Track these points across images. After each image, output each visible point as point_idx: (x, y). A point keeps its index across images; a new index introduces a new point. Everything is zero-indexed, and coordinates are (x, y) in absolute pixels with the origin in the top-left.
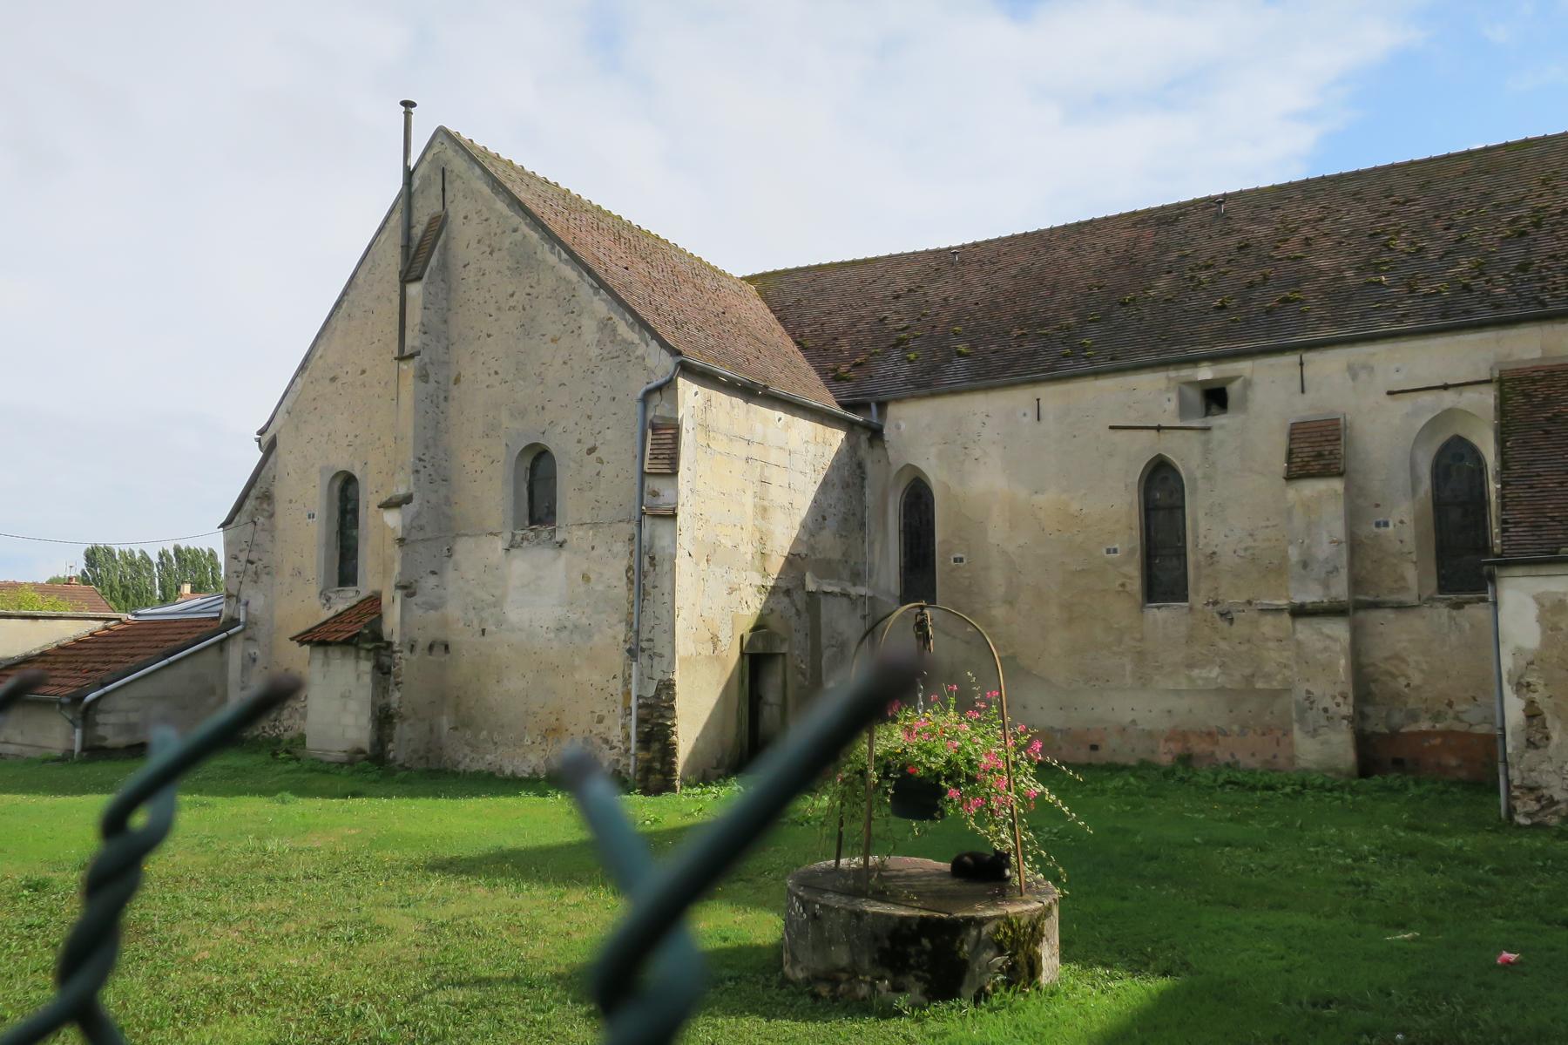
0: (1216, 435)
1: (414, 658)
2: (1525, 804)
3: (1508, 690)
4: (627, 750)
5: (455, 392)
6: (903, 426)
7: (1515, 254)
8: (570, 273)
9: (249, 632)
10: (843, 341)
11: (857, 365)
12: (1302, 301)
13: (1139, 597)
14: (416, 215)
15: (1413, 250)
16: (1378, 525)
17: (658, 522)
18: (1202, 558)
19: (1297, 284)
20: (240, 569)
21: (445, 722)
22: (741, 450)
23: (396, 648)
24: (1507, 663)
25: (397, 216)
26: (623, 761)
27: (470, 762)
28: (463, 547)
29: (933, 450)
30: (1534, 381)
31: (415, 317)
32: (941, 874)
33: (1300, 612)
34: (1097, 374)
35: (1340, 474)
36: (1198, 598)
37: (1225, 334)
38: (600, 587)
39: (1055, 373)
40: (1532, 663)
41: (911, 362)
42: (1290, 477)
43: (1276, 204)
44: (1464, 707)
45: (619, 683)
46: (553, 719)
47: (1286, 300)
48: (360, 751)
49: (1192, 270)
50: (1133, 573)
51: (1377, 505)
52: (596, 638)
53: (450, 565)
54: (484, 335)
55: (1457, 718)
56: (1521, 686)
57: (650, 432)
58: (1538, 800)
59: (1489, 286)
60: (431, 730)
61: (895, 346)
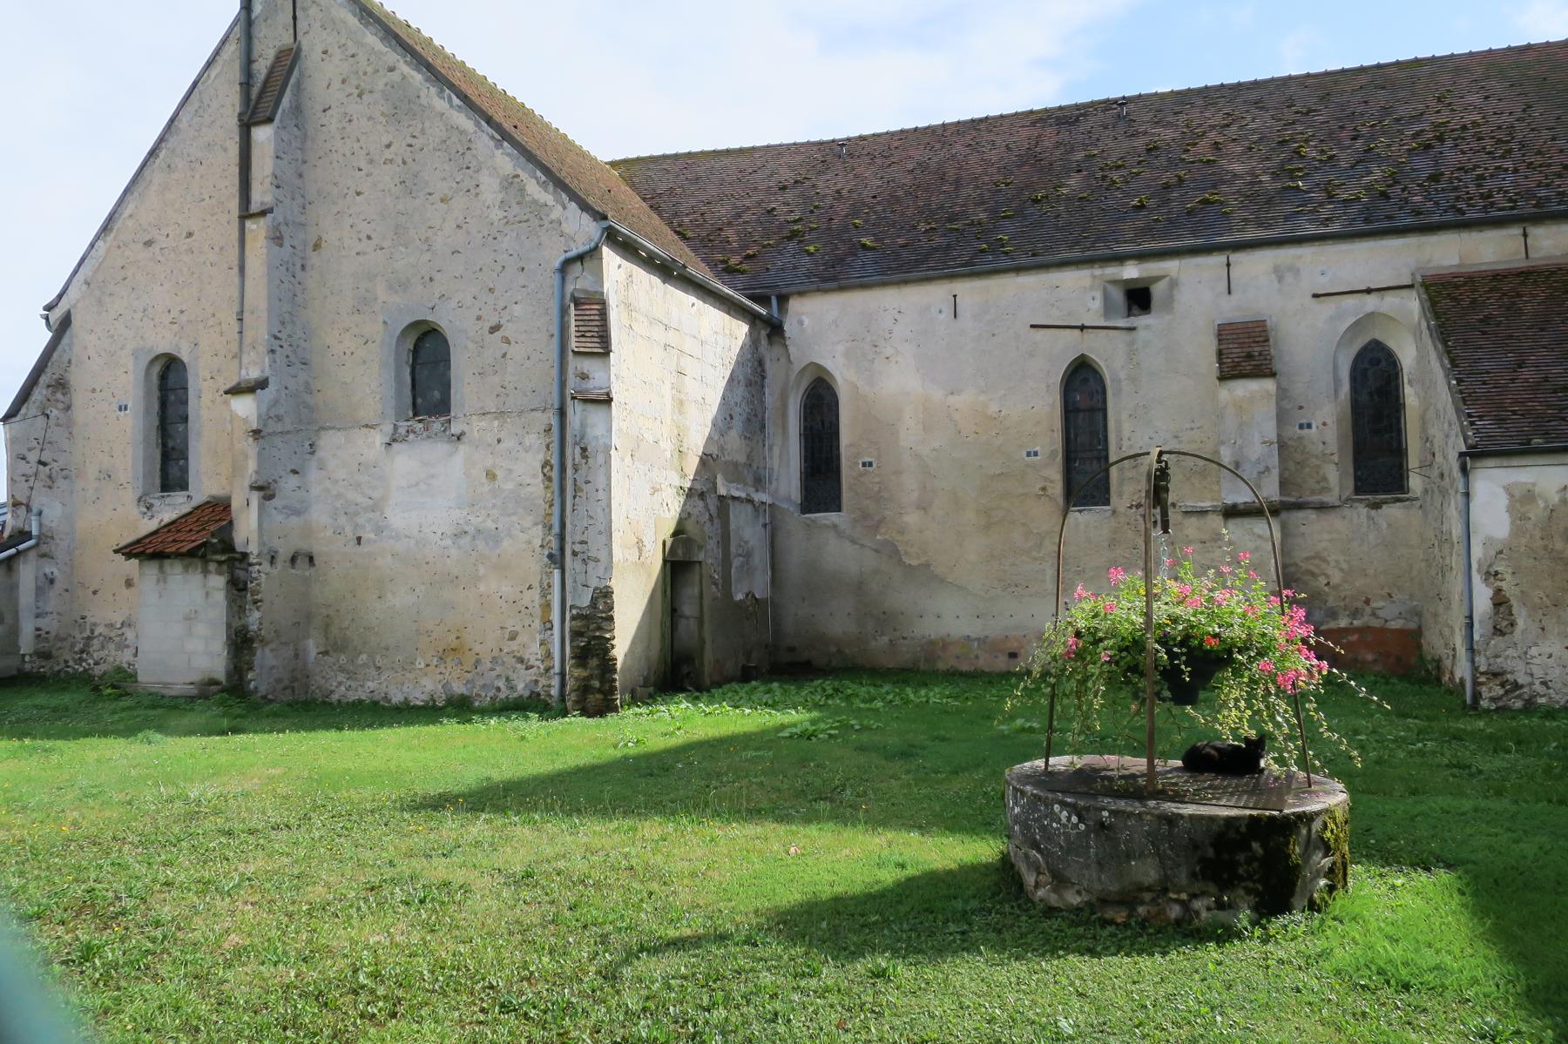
0: (1141, 335)
1: (275, 572)
2: (1490, 689)
3: (1477, 579)
4: (547, 670)
5: (314, 259)
6: (806, 322)
7: (1424, 165)
8: (464, 121)
9: (44, 548)
10: (730, 233)
11: (748, 257)
12: (1222, 203)
13: (1061, 501)
14: (258, 47)
15: (1324, 158)
16: (1301, 427)
17: (590, 407)
19: (1214, 186)
20: (30, 472)
21: (312, 647)
22: (658, 333)
23: (252, 560)
24: (1477, 552)
25: (232, 48)
26: (543, 681)
27: (343, 690)
28: (329, 442)
29: (840, 348)
30: (1457, 287)
31: (263, 166)
32: (1177, 769)
33: (1231, 512)
34: (1018, 270)
35: (1273, 375)
37: (1147, 232)
38: (510, 486)
39: (974, 268)
40: (1501, 552)
41: (810, 254)
42: (1224, 377)
43: (1177, 109)
44: (1381, 604)
45: (535, 595)
46: (453, 637)
47: (1206, 202)
48: (213, 682)
49: (1102, 169)
50: (1055, 474)
51: (1301, 408)
52: (506, 543)
53: (313, 464)
54: (352, 192)
55: (1374, 614)
56: (1491, 575)
57: (572, 311)
58: (1502, 685)
59: (1405, 194)
60: (297, 656)
61: (789, 239)
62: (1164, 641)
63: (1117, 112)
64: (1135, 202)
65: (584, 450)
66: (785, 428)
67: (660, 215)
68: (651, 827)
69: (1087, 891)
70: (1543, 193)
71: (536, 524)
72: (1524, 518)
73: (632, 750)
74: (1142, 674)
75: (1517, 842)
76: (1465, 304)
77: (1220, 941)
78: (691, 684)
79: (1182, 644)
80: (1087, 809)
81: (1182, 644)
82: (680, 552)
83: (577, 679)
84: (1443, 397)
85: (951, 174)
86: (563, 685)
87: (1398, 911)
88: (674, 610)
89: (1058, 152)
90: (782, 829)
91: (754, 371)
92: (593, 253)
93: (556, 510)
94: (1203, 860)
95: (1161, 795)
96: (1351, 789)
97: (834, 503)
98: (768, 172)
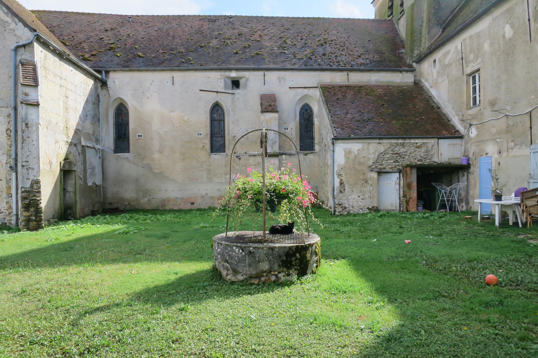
0: (236, 96)
3: (336, 176)
4: (10, 213)
7: (321, 50)
10: (85, 45)
11: (92, 55)
12: (262, 55)
13: (209, 151)
16: (285, 129)
17: (29, 107)
18: (230, 137)
19: (260, 49)
24: (336, 168)
30: (330, 89)
34: (196, 70)
35: (277, 112)
36: (229, 151)
37: (238, 61)
39: (179, 68)
41: (118, 57)
43: (248, 22)
47: (257, 54)
50: (207, 142)
56: (340, 175)
62: (268, 191)
63: (229, 19)
64: (235, 51)
65: (27, 124)
66: (107, 121)
67: (54, 34)
68: (73, 269)
69: (245, 274)
70: (353, 63)
71: (3, 154)
72: (348, 158)
73: (55, 242)
74: (261, 202)
75: (359, 250)
76: (332, 94)
77: (289, 286)
78: (72, 217)
79: (273, 192)
80: (245, 247)
81: (273, 192)
82: (67, 166)
83: (25, 216)
84: (327, 121)
85: (171, 34)
86: (17, 219)
87: (333, 272)
88: (64, 189)
89: (209, 31)
90: (127, 265)
91: (96, 99)
92: (30, 44)
93: (13, 148)
94: (282, 261)
95: (266, 241)
96: (320, 235)
97: (127, 149)
98: (100, 24)
